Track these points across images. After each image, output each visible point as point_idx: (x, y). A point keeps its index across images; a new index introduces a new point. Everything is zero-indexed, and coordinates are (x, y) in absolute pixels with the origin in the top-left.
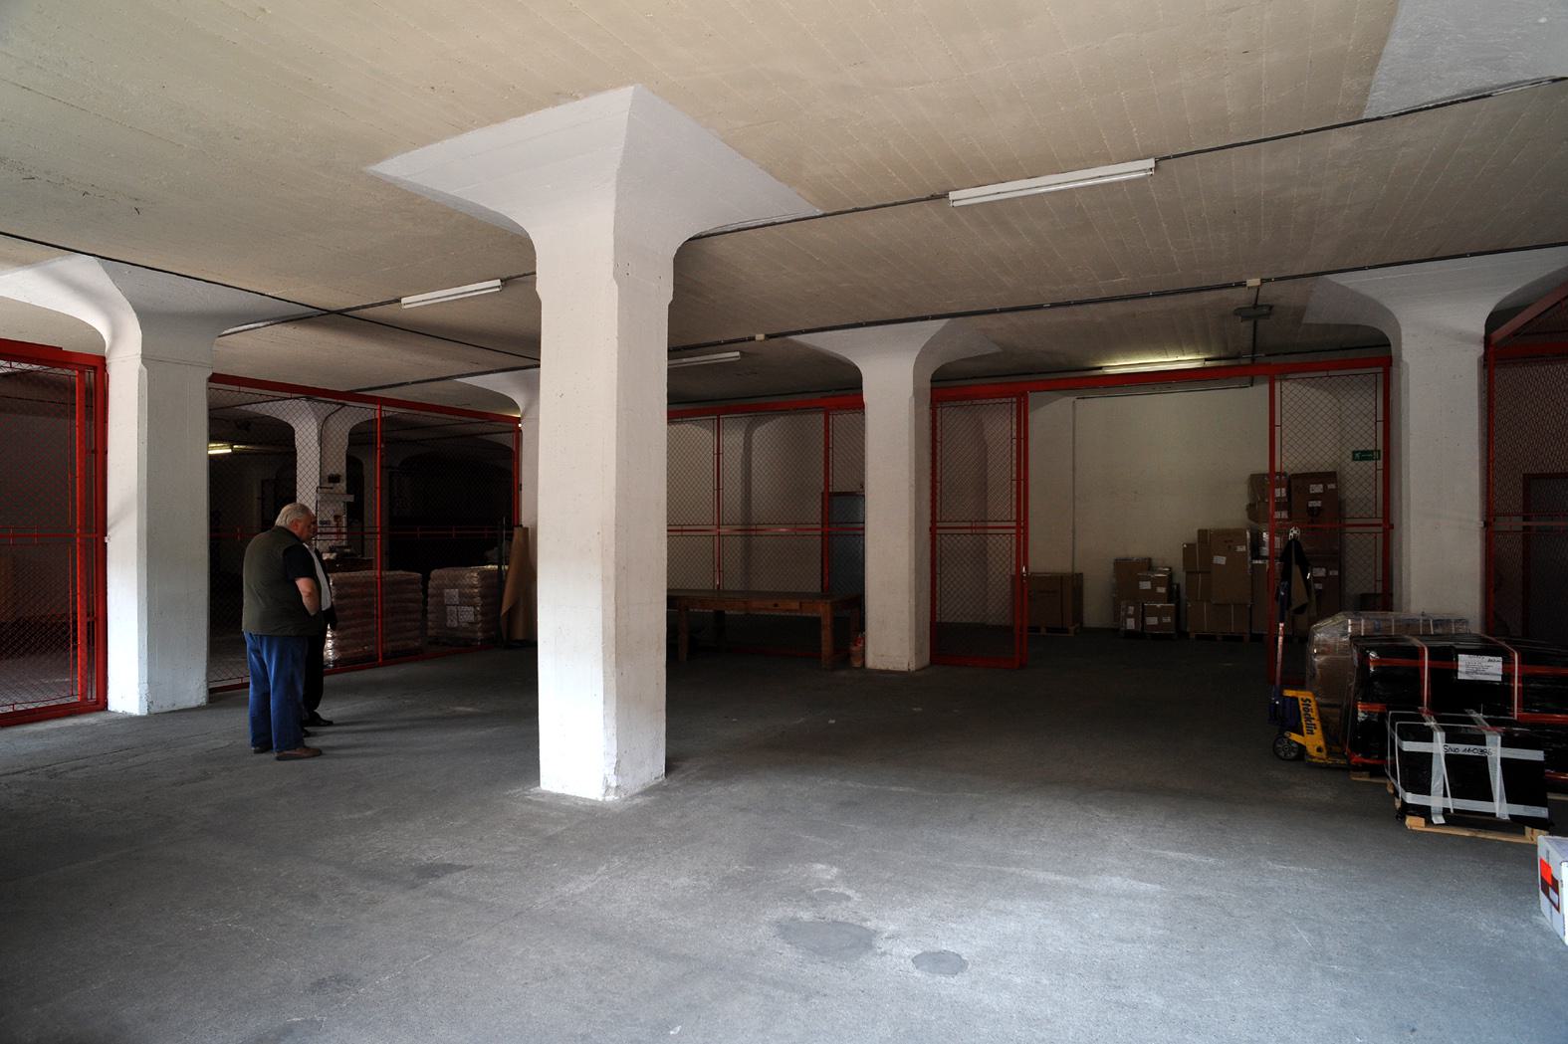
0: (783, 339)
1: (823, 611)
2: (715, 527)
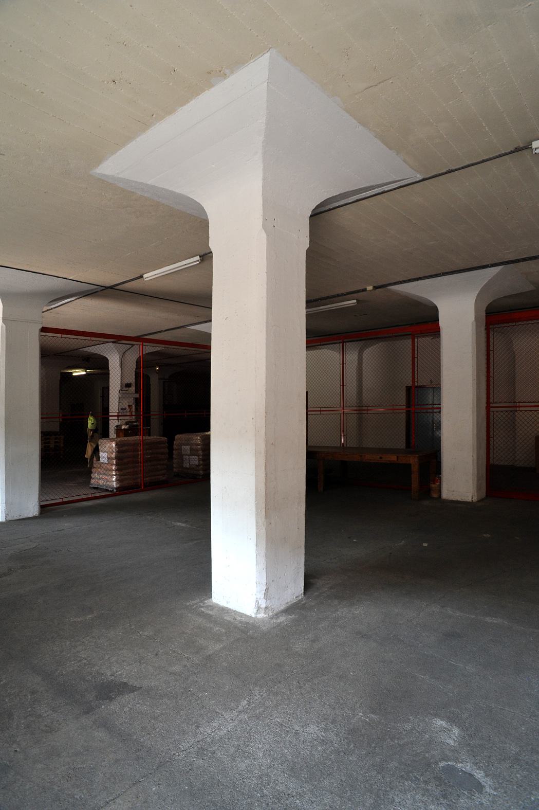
0: (384, 289)
1: (413, 461)
2: (341, 408)
